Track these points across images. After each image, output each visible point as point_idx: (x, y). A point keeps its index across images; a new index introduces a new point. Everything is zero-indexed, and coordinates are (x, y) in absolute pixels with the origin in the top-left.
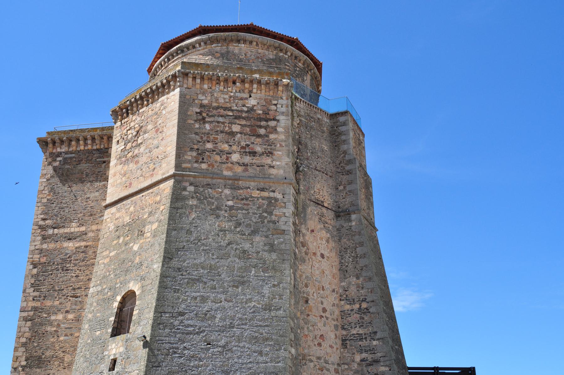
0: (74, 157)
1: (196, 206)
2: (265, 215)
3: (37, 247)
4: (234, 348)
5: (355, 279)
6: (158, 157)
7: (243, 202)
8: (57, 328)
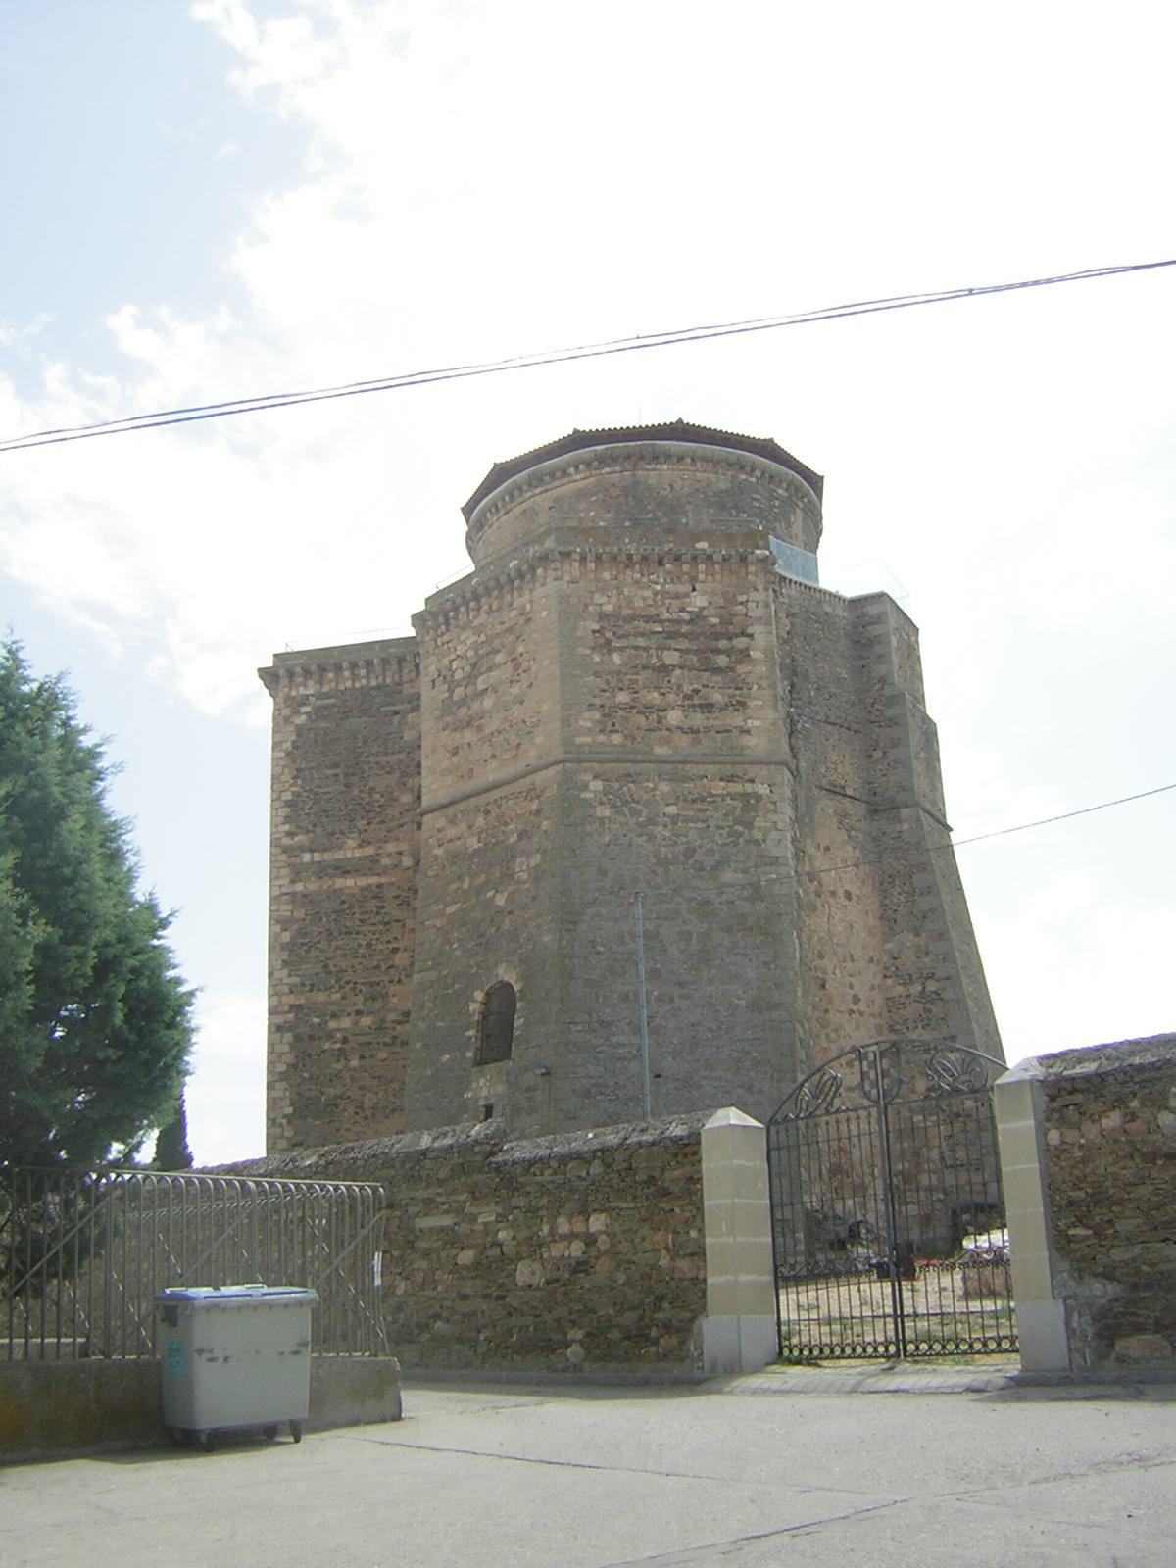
0: (334, 705)
2: (740, 828)
3: (283, 890)
4: (703, 1082)
5: (911, 936)
7: (695, 806)
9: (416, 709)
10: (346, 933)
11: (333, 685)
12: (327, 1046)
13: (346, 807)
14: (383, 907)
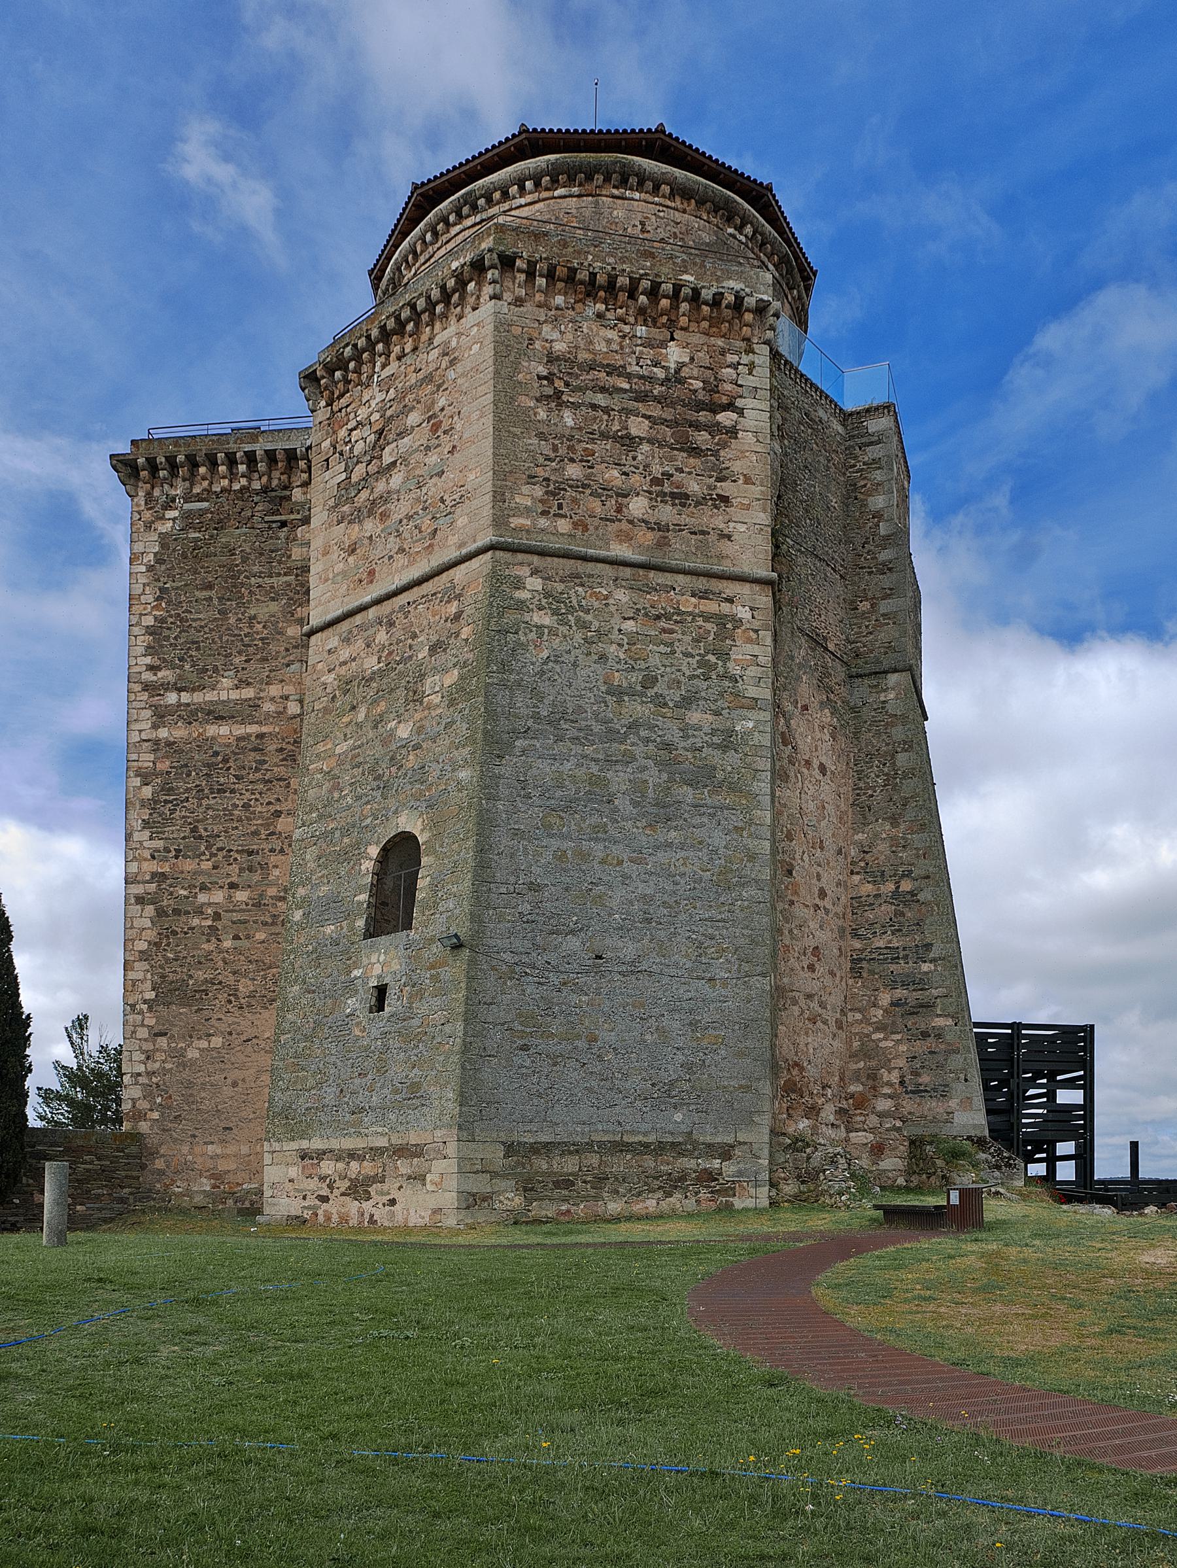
0: (207, 511)
1: (550, 629)
2: (712, 658)
6: (442, 501)
8: (213, 920)
9: (306, 521)
10: (219, 791)
11: (206, 484)
12: (196, 922)
13: (221, 638)
14: (265, 762)
